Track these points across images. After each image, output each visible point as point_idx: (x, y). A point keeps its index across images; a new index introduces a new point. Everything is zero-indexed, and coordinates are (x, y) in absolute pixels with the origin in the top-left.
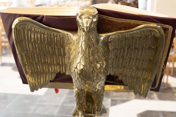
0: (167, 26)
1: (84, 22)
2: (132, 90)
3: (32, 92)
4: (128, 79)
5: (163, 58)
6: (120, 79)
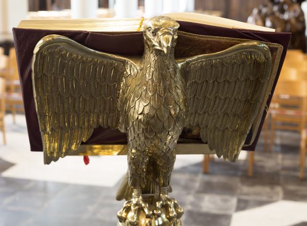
0: (275, 45)
1: (164, 42)
2: (214, 150)
3: (46, 165)
4: (209, 133)
5: (266, 95)
6: (195, 134)
